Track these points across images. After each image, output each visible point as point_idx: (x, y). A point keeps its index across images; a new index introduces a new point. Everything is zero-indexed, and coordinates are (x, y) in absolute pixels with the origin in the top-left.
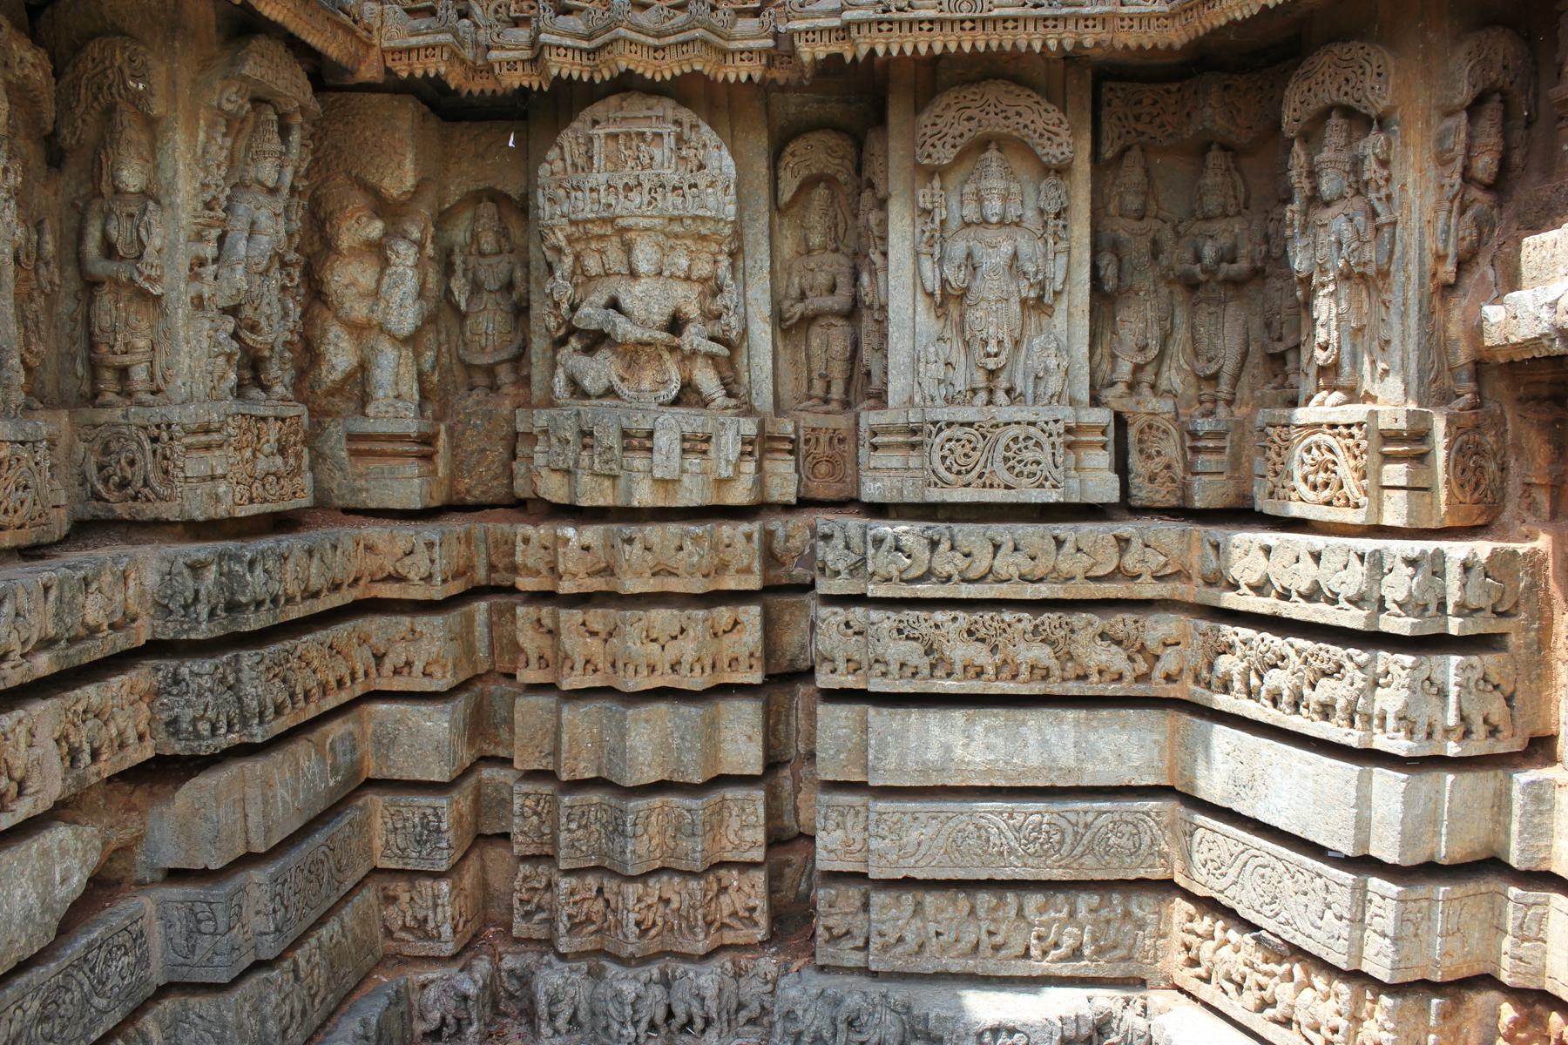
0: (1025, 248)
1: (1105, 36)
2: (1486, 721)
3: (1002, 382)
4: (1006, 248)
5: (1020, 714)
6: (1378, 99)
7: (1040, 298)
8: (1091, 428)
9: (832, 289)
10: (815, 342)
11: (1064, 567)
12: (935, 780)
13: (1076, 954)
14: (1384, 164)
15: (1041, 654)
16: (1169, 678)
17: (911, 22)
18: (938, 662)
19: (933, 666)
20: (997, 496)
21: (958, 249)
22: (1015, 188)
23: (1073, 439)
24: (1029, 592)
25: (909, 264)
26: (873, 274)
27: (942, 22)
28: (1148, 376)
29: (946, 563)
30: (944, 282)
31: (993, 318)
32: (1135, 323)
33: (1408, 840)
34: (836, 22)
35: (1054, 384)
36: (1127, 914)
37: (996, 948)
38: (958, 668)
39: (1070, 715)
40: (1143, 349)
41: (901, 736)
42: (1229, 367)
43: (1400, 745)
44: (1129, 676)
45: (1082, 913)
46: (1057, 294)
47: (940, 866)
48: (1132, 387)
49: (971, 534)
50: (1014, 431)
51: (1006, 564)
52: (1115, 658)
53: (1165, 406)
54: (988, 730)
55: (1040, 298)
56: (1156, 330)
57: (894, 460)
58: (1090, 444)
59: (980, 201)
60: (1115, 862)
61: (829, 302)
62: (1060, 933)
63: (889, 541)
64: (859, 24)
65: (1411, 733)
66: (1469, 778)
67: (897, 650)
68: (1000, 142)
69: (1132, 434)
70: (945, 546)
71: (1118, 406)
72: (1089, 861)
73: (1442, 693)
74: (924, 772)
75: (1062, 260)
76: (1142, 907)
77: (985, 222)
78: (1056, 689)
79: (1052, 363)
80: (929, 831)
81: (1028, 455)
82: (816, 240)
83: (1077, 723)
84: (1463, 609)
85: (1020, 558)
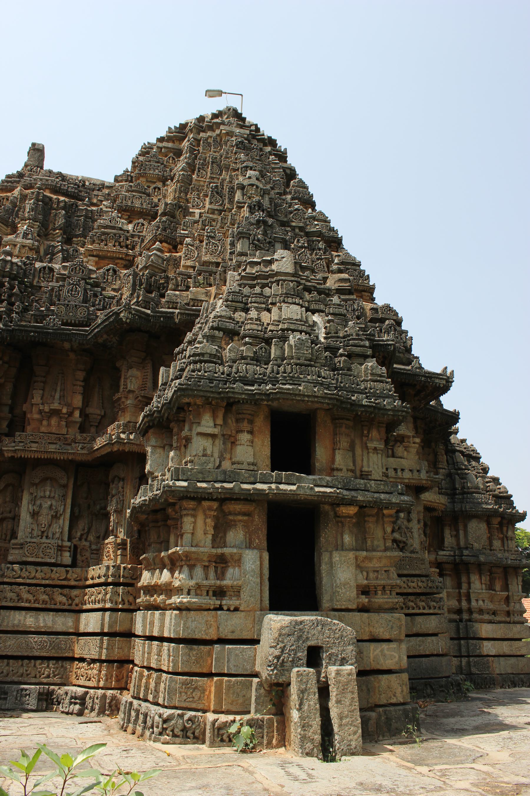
0: (54, 503)
1: (74, 457)
2: (128, 601)
3: (45, 534)
4: (49, 503)
5: (39, 613)
6: (122, 475)
7: (56, 515)
8: (66, 547)
9: (10, 512)
10: (4, 525)
11: (53, 576)
12: (16, 629)
13: (48, 676)
14: (123, 488)
15: (45, 597)
16: (77, 605)
17: (30, 451)
18: (20, 599)
19: (18, 600)
20: (39, 560)
21: (38, 502)
22: (53, 489)
23: (60, 549)
24: (44, 582)
25: (27, 505)
26: (19, 508)
27: (37, 451)
28: (85, 537)
29: (24, 574)
30: (34, 510)
31: (44, 520)
32: (82, 524)
33: (110, 626)
34: (13, 449)
35: (57, 535)
36: (62, 666)
37: (28, 675)
38: (25, 600)
39: (51, 613)
40: (84, 530)
41: (9, 617)
42: (102, 535)
43: (108, 605)
44: (67, 604)
45: (51, 665)
46: (61, 515)
47: (15, 651)
48: (80, 539)
49: (31, 568)
50: (45, 545)
51: (39, 575)
52: (64, 599)
53: (87, 544)
54: (30, 616)
55: (56, 515)
56: (87, 526)
57: (17, 552)
58: (65, 551)
59: (45, 492)
60: (60, 652)
61: (9, 515)
62: (44, 671)
63: (11, 568)
64: (18, 450)
65: (112, 603)
66: (124, 614)
67: (10, 595)
68: (51, 479)
69: (79, 550)
70: (24, 570)
71: (75, 543)
72: (53, 651)
73: (119, 595)
74: (13, 626)
75: (63, 507)
76: (67, 664)
77: (45, 497)
78: (48, 606)
79: (57, 530)
80: (13, 642)
81: (48, 551)
82: (8, 499)
83: (53, 615)
84: (123, 576)
85: (42, 574)
